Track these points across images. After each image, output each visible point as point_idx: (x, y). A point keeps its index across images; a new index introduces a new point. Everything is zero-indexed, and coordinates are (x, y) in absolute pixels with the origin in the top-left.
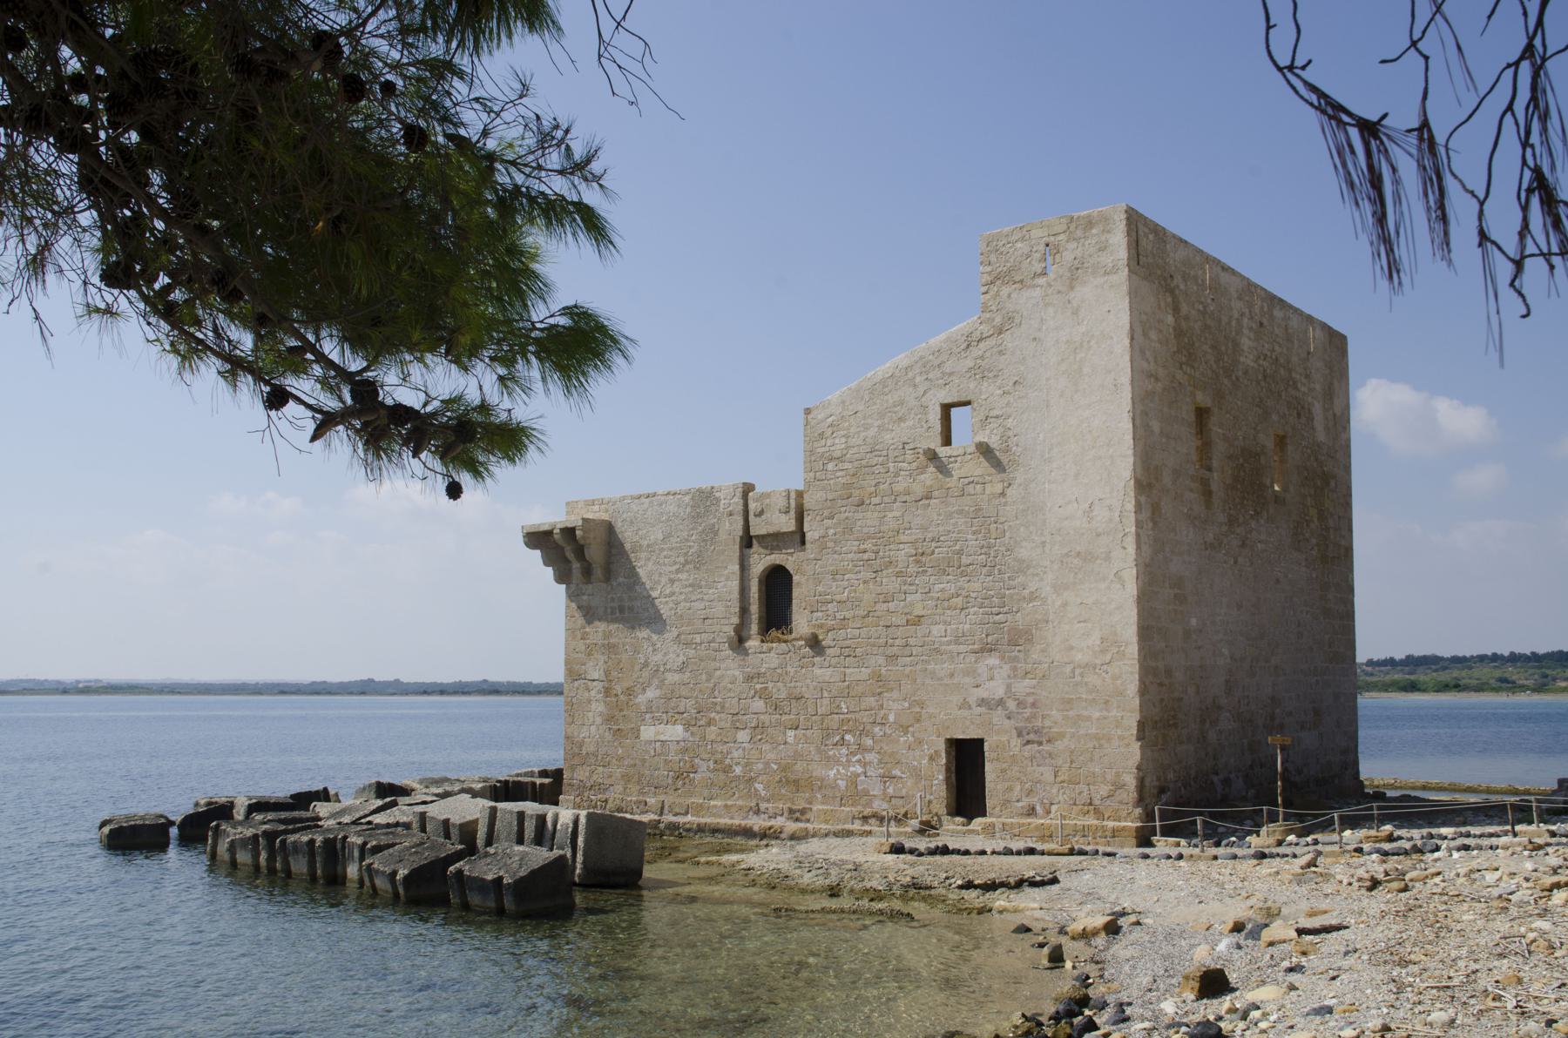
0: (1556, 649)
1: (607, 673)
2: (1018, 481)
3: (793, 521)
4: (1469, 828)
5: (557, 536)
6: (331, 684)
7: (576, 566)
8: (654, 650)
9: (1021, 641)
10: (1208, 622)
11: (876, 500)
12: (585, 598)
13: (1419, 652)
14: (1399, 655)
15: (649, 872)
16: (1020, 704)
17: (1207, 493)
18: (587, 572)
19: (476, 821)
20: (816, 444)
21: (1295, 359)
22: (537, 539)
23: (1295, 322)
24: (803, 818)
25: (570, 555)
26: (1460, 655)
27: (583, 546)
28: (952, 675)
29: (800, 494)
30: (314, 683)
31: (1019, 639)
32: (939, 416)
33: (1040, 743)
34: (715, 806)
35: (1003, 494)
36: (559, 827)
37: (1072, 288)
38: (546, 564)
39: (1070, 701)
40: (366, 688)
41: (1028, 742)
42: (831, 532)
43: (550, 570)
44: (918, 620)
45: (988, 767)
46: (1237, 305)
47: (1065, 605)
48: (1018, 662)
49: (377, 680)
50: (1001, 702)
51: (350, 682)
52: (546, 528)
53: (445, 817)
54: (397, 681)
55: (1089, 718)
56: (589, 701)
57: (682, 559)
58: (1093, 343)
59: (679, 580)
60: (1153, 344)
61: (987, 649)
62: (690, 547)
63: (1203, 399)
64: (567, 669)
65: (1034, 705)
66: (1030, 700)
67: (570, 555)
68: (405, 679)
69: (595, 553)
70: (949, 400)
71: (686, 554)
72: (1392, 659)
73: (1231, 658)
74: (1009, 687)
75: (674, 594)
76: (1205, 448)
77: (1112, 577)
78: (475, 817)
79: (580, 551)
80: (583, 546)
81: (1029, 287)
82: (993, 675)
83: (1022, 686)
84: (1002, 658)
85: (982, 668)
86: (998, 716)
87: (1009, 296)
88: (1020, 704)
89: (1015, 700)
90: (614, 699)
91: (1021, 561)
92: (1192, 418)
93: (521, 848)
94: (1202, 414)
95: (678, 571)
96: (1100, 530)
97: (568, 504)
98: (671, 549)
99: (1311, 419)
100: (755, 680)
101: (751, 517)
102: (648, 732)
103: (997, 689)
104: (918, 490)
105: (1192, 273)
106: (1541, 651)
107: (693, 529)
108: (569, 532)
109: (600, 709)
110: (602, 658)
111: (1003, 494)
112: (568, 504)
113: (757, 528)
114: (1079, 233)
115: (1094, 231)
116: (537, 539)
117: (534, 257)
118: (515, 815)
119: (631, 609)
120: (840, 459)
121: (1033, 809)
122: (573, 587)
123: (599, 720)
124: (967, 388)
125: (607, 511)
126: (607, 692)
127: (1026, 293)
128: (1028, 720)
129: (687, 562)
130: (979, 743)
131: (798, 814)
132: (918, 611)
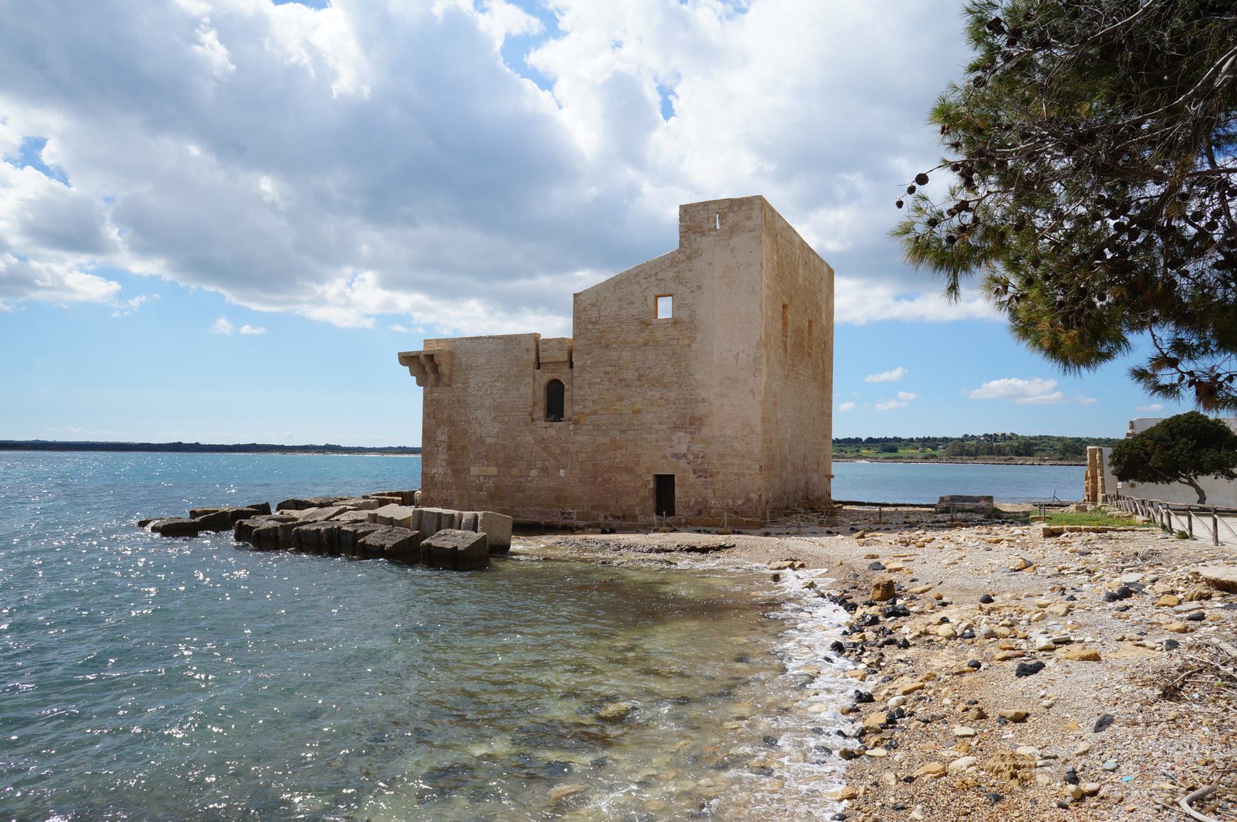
0: (847, 437)
1: (449, 438)
4: (586, 536)
5: (422, 360)
9: (697, 423)
11: (614, 346)
12: (436, 394)
15: (512, 548)
16: (696, 456)
17: (786, 350)
20: (581, 314)
21: (817, 281)
22: (408, 359)
23: (817, 261)
25: (428, 369)
26: (853, 437)
27: (437, 365)
28: (657, 442)
33: (706, 477)
35: (689, 346)
36: (463, 521)
37: (731, 238)
39: (723, 455)
40: (177, 447)
41: (699, 477)
42: (589, 362)
43: (414, 379)
44: (639, 412)
45: (677, 490)
46: (798, 251)
47: (722, 405)
50: (685, 456)
54: (197, 444)
55: (733, 465)
57: (497, 375)
61: (677, 428)
63: (786, 301)
65: (703, 457)
66: (701, 455)
67: (428, 369)
68: (202, 442)
69: (444, 369)
71: (500, 372)
74: (689, 447)
76: (785, 324)
79: (435, 368)
80: (437, 365)
82: (681, 442)
83: (697, 448)
84: (686, 433)
85: (675, 437)
86: (683, 463)
90: (454, 452)
93: (460, 531)
94: (785, 306)
95: (494, 381)
97: (425, 341)
99: (821, 313)
102: (474, 470)
104: (640, 341)
106: (840, 438)
108: (430, 357)
110: (446, 429)
111: (689, 346)
112: (425, 341)
114: (736, 209)
115: (744, 208)
116: (408, 359)
119: (465, 401)
120: (594, 323)
122: (428, 388)
123: (444, 464)
126: (450, 448)
127: (704, 238)
128: (700, 465)
129: (500, 376)
132: (639, 406)
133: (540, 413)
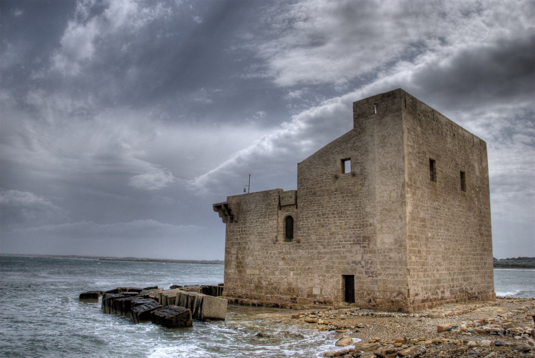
2: (366, 184)
3: (294, 201)
6: (207, 261)
7: (229, 217)
8: (251, 244)
10: (435, 235)
13: (522, 256)
14: (516, 257)
18: (232, 219)
19: (175, 297)
22: (217, 207)
24: (295, 301)
29: (296, 192)
30: (203, 261)
31: (367, 239)
32: (340, 164)
34: (268, 297)
38: (220, 216)
48: (366, 248)
49: (220, 260)
50: (360, 262)
51: (212, 261)
52: (220, 205)
53: (167, 295)
56: (232, 261)
58: (390, 136)
59: (259, 221)
60: (412, 136)
62: (262, 210)
64: (225, 250)
70: (344, 158)
71: (261, 213)
72: (514, 258)
73: (445, 248)
74: (363, 257)
75: (257, 225)
77: (398, 217)
78: (174, 296)
79: (229, 211)
81: (369, 118)
87: (362, 122)
88: (367, 263)
89: (364, 261)
90: (239, 260)
91: (367, 213)
92: (429, 163)
95: (259, 218)
96: (394, 201)
98: (257, 211)
100: (281, 254)
101: (281, 199)
103: (358, 258)
104: (333, 188)
105: (427, 114)
107: (263, 204)
109: (235, 263)
113: (283, 204)
116: (217, 207)
117: (63, 36)
118: (186, 296)
121: (370, 300)
123: (234, 267)
124: (350, 154)
125: (238, 199)
130: (353, 276)
131: (293, 300)
133: (281, 238)
